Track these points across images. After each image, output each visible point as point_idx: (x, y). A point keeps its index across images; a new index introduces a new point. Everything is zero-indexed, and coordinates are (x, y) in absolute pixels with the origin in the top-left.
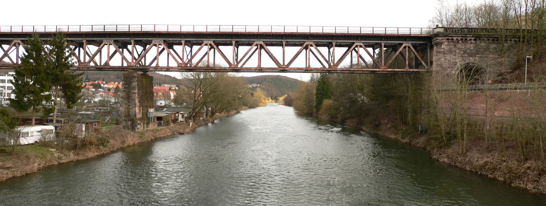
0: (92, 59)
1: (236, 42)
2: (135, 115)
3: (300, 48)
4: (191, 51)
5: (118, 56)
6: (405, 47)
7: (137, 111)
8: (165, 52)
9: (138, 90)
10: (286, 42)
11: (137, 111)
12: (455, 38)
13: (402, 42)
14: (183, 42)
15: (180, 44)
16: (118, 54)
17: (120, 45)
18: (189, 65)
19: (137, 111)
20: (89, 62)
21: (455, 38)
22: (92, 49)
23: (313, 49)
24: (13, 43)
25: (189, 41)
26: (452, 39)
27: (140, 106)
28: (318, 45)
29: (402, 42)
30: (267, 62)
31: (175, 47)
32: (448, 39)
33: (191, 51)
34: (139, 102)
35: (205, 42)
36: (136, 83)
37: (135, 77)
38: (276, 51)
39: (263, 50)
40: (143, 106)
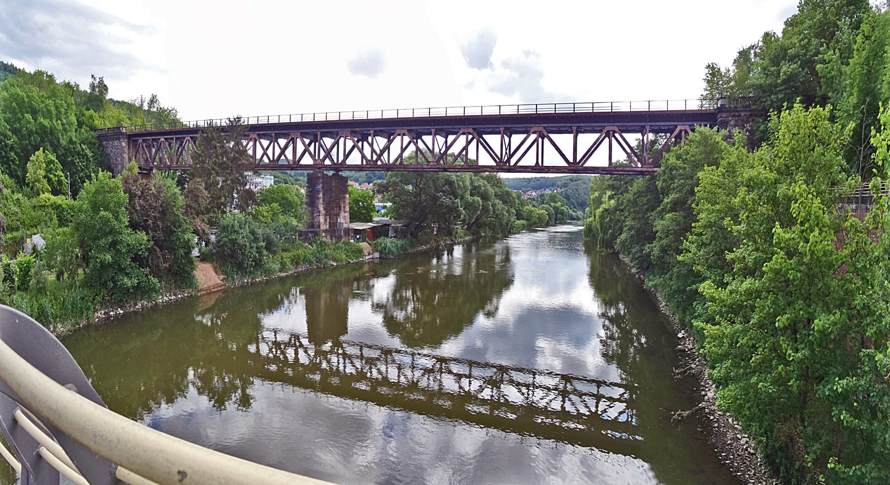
0: (328, 154)
1: (321, 133)
2: (319, 226)
3: (597, 135)
4: (446, 142)
5: (412, 147)
6: (681, 131)
7: (322, 220)
8: (475, 141)
9: (324, 194)
10: (578, 127)
11: (323, 222)
12: (743, 114)
13: (676, 123)
14: (433, 131)
15: (429, 134)
16: (412, 144)
17: (414, 135)
18: (441, 162)
19: (322, 220)
20: (324, 159)
21: (743, 114)
22: (380, 142)
23: (617, 135)
24: (605, 131)
25: (441, 130)
26: (740, 115)
27: (325, 215)
28: (622, 131)
29: (676, 123)
30: (552, 158)
31: (424, 137)
32: (734, 116)
33: (446, 142)
34: (325, 209)
35: (398, 132)
36: (321, 185)
37: (319, 178)
38: (564, 141)
39: (546, 140)
40: (330, 215)
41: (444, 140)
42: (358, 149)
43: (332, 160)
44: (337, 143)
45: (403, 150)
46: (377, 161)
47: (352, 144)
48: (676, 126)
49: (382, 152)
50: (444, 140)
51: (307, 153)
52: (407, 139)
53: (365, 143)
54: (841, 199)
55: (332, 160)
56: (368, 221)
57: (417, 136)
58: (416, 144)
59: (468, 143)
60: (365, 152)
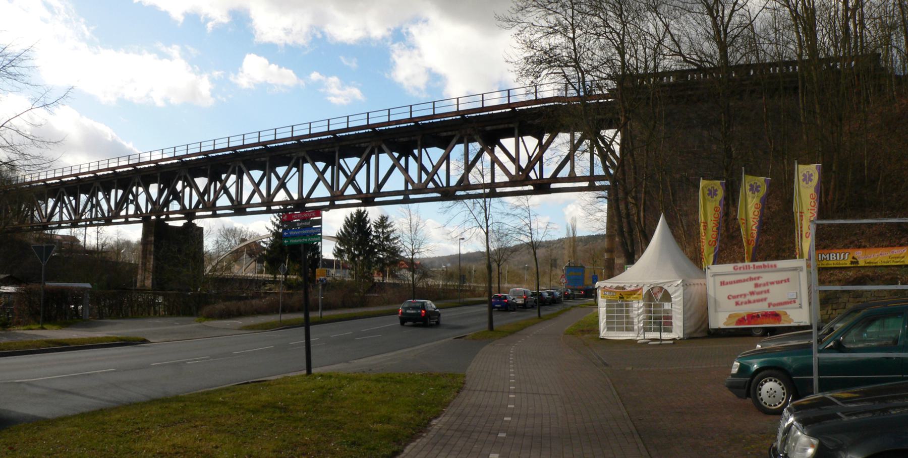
31: (504, 141)
41: (536, 141)
42: (401, 168)
43: (261, 195)
44: (446, 158)
45: (469, 167)
46: (427, 183)
47: (391, 163)
48: (34, 247)
49: (436, 168)
50: (536, 141)
51: (397, 169)
52: (475, 147)
53: (411, 159)
54: (646, 62)
55: (261, 195)
56: (628, 330)
57: (490, 141)
58: (492, 152)
59: (574, 148)
60: (565, 151)
